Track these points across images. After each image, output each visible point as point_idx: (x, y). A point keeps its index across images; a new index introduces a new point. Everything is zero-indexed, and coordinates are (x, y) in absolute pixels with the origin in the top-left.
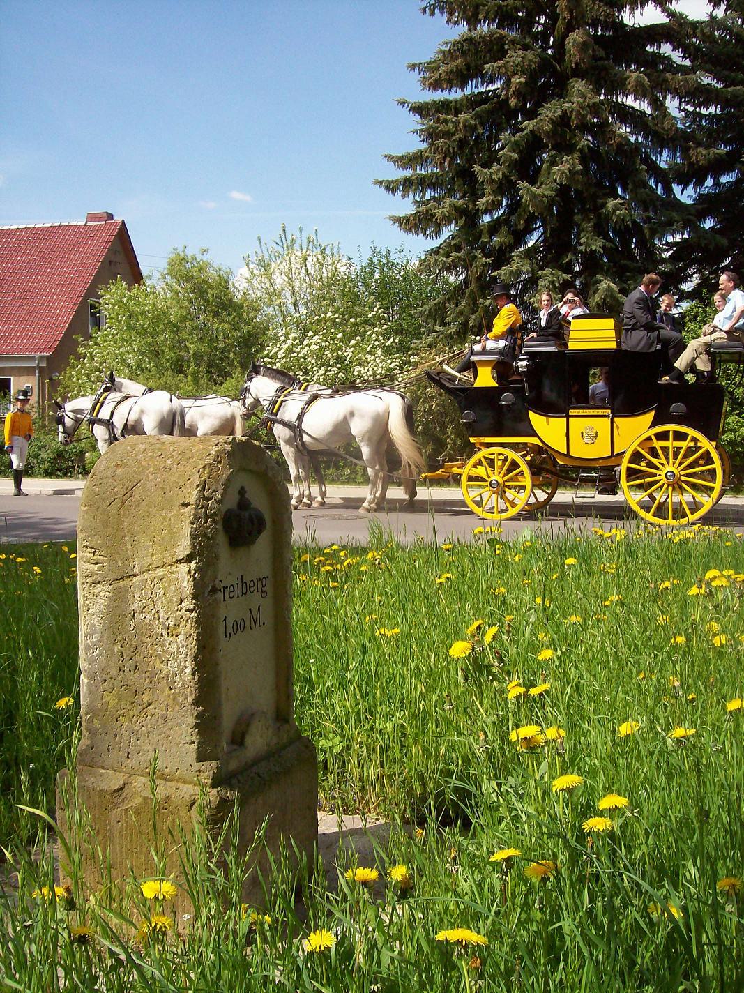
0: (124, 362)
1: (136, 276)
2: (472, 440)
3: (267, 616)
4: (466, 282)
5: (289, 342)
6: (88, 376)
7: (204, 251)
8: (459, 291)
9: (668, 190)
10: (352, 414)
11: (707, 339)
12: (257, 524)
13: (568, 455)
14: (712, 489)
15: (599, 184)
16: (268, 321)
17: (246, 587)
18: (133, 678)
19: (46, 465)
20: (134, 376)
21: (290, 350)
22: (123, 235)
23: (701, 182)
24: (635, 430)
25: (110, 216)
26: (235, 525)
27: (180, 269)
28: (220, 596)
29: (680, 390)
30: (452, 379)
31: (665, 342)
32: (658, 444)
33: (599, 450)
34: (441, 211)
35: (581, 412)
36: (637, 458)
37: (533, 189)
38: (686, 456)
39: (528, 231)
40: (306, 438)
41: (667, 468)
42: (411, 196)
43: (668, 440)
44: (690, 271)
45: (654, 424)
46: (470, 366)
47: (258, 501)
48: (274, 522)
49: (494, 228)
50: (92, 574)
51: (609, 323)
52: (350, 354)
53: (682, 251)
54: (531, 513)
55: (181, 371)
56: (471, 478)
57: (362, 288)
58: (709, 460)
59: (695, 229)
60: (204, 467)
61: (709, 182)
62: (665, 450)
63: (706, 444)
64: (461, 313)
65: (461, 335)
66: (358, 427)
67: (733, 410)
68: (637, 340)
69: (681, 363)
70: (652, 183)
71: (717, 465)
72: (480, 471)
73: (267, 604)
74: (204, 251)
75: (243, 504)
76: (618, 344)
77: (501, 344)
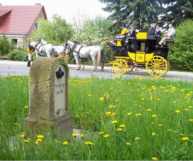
0: (42, 37)
1: (46, 18)
2: (116, 57)
3: (64, 91)
4: (117, 23)
5: (78, 34)
6: (34, 39)
7: (60, 13)
8: (115, 25)
9: (161, 5)
10: (90, 50)
11: (166, 38)
12: (63, 74)
13: (135, 61)
14: (165, 70)
15: (147, 3)
16: (74, 29)
17: (60, 86)
18: (38, 101)
19: (25, 59)
20: (44, 40)
21: (78, 36)
22: (43, 9)
23: (168, 4)
24: (150, 57)
25: (40, 4)
26: (58, 74)
27: (55, 17)
28: (55, 87)
29: (159, 49)
30: (112, 44)
31: (157, 38)
32: (154, 60)
33: (142, 60)
34: (112, 7)
35: (139, 52)
36: (150, 62)
37: (132, 4)
38: (160, 62)
39: (131, 12)
40: (80, 55)
41: (157, 65)
42: (106, 3)
43: (156, 59)
44: (165, 23)
45: (153, 56)
46: (116, 42)
47: (63, 69)
48: (66, 74)
49: (123, 11)
50: (32, 82)
51: (146, 33)
52: (91, 37)
53: (164, 19)
54: (127, 73)
55: (54, 39)
56: (115, 65)
57: (95, 23)
58: (165, 64)
59: (166, 14)
60: (53, 63)
61: (170, 4)
62: (156, 61)
63: (164, 60)
64: (115, 29)
65: (115, 34)
66: (91, 53)
67: (172, 53)
68: (152, 38)
69: (160, 43)
70: (158, 3)
71: (166, 65)
72: (118, 64)
73: (64, 89)
74: (60, 13)
75: (60, 70)
76: (147, 38)
77: (123, 37)
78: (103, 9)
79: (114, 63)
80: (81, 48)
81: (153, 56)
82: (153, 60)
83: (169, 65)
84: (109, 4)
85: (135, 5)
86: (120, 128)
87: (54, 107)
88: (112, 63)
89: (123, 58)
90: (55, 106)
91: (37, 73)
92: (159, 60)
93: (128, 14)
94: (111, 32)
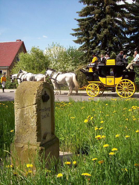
1: (25, 51)
2: (88, 82)
3: (50, 115)
5: (54, 64)
6: (16, 70)
7: (38, 47)
8: (86, 54)
9: (125, 35)
10: (66, 77)
11: (132, 63)
12: (48, 98)
13: (106, 85)
14: (133, 91)
15: (112, 34)
17: (46, 110)
19: (9, 87)
20: (25, 70)
22: (23, 43)
23: (131, 34)
24: (119, 80)
25: (21, 40)
26: (44, 98)
27: (34, 50)
28: (41, 111)
29: (127, 73)
30: (84, 71)
31: (124, 64)
32: (123, 83)
33: (112, 84)
35: (109, 77)
36: (119, 85)
39: (99, 43)
42: (77, 36)
44: (129, 51)
45: (122, 79)
46: (88, 68)
47: (48, 93)
48: (51, 97)
49: (92, 42)
51: (114, 60)
54: (99, 96)
55: (34, 69)
56: (88, 89)
58: (133, 86)
61: (132, 34)
63: (132, 83)
64: (86, 58)
65: (86, 62)
66: (67, 80)
67: (137, 76)
68: (119, 63)
69: (127, 68)
70: (122, 34)
71: (134, 87)
72: (90, 88)
74: (38, 47)
75: (45, 94)
76: (115, 64)
78: (74, 41)
79: (87, 87)
80: (58, 75)
81: (122, 79)
82: (121, 83)
83: (136, 87)
84: (80, 37)
85: (102, 36)
86: (112, 152)
87: (41, 131)
88: (85, 88)
89: (94, 83)
90: (42, 130)
91: (22, 97)
92: (127, 83)
93: (97, 44)
94: (83, 60)
